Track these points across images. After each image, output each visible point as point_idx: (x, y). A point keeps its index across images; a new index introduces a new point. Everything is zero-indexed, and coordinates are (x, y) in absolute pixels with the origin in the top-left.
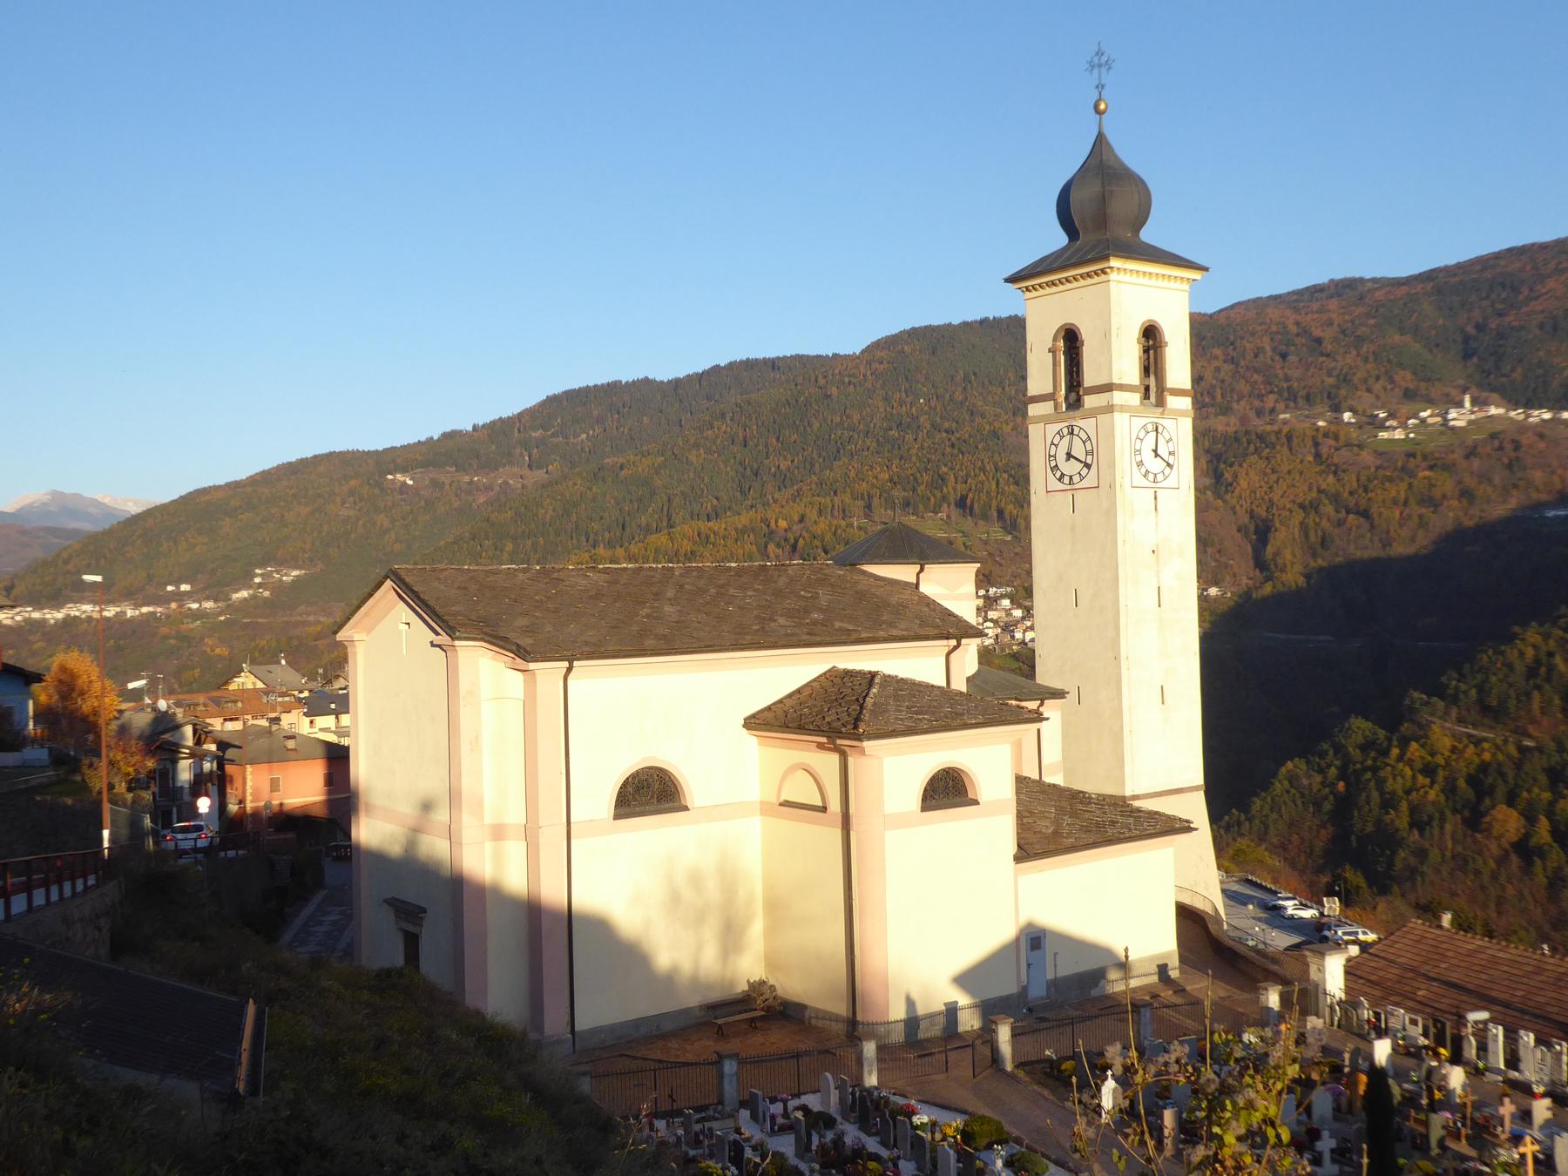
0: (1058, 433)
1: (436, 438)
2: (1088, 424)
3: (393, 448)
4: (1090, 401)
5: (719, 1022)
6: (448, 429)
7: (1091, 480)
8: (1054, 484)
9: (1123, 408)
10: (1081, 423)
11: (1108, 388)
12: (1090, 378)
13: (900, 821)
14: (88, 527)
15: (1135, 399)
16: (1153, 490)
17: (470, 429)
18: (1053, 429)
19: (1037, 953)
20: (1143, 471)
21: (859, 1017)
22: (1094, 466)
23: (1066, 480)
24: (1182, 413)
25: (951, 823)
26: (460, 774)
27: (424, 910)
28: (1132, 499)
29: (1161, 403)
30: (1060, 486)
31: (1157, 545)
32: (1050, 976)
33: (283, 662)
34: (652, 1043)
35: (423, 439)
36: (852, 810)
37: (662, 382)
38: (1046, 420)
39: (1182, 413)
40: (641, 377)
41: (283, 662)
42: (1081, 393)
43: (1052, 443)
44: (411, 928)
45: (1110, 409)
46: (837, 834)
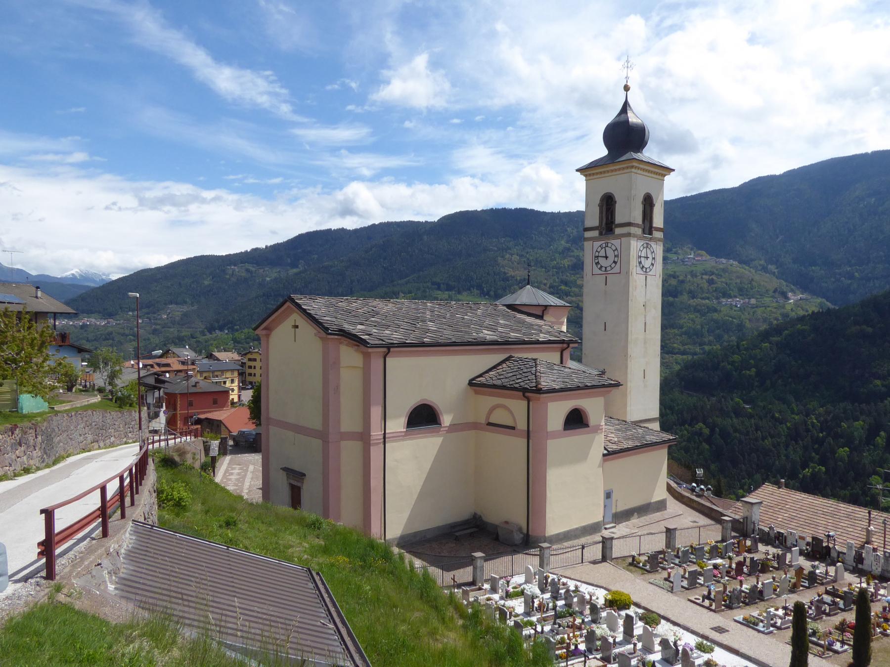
0: (600, 246)
1: (249, 251)
2: (616, 242)
3: (230, 255)
4: (618, 231)
5: (457, 534)
6: (254, 247)
7: (617, 269)
8: (596, 271)
9: (635, 236)
10: (613, 242)
11: (629, 224)
12: (619, 219)
13: (555, 435)
14: (93, 285)
15: (639, 231)
16: (604, 276)
17: (264, 247)
18: (597, 244)
19: (609, 500)
20: (599, 266)
21: (530, 533)
22: (618, 264)
23: (603, 269)
24: (659, 240)
25: (577, 438)
26: (510, 435)
27: (304, 475)
28: (637, 278)
29: (650, 233)
30: (600, 272)
31: (645, 302)
32: (614, 511)
33: (187, 347)
34: (424, 545)
35: (243, 251)
36: (531, 429)
37: (350, 230)
38: (593, 239)
39: (659, 240)
40: (340, 227)
41: (187, 347)
42: (613, 227)
43: (597, 251)
44: (295, 483)
45: (629, 235)
46: (526, 440)
